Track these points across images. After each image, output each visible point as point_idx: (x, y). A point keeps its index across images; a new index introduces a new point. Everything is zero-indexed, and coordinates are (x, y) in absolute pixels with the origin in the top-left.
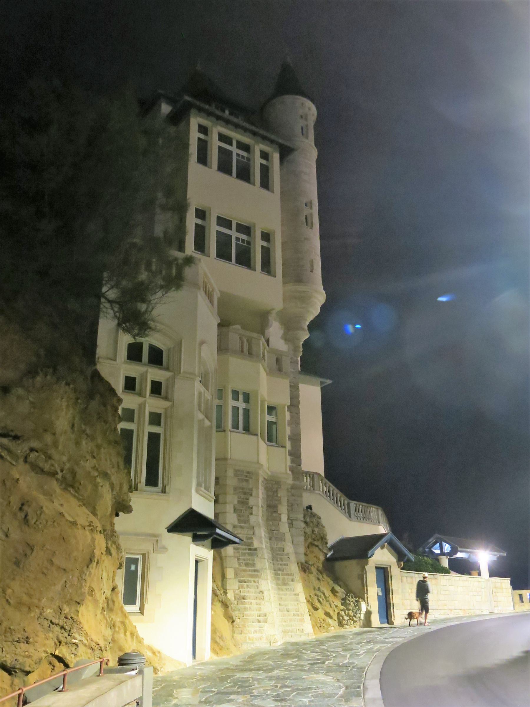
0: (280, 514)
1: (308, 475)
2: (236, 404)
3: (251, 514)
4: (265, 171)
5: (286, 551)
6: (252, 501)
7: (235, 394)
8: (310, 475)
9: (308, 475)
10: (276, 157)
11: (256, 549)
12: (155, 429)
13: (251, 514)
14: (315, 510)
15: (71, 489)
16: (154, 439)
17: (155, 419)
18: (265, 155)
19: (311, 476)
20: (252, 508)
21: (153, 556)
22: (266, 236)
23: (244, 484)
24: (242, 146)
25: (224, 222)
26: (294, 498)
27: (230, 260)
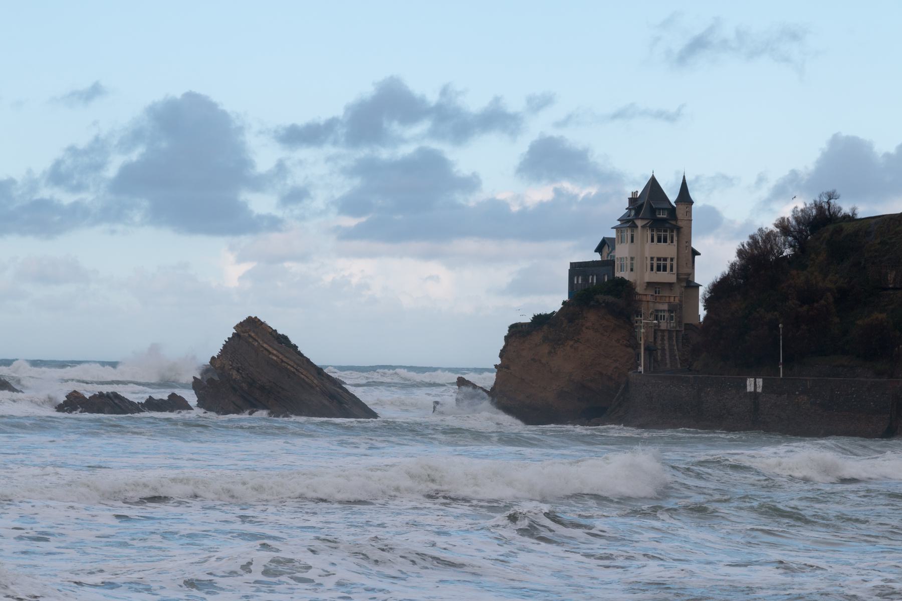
22: (672, 259)
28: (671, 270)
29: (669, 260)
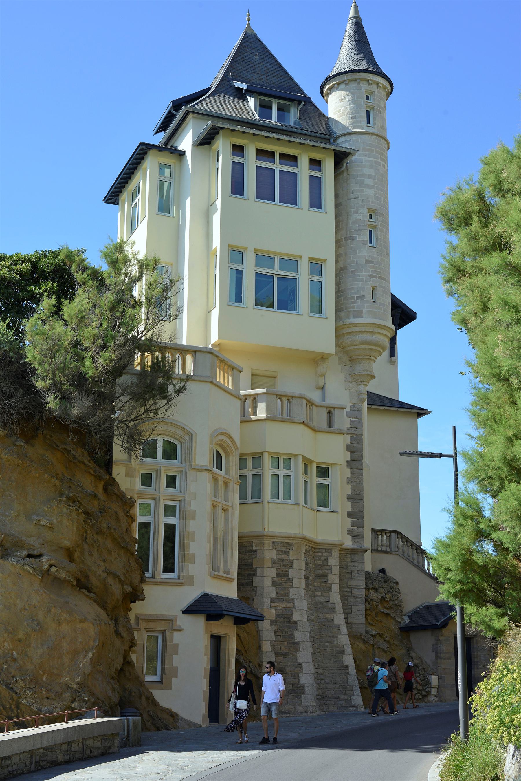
0: (331, 584)
1: (383, 534)
2: (276, 472)
3: (292, 586)
4: (316, 184)
5: (336, 622)
6: (292, 573)
7: (275, 458)
8: (386, 533)
9: (383, 534)
10: (329, 165)
11: (295, 622)
12: (170, 521)
13: (292, 586)
14: (390, 572)
15: (84, 590)
16: (170, 530)
17: (170, 511)
18: (316, 163)
19: (388, 534)
20: (292, 580)
21: (168, 633)
22: (316, 266)
23: (283, 557)
24: (285, 158)
25: (263, 258)
26: (353, 564)
27: (271, 306)
28: (317, 308)
29: (304, 267)
